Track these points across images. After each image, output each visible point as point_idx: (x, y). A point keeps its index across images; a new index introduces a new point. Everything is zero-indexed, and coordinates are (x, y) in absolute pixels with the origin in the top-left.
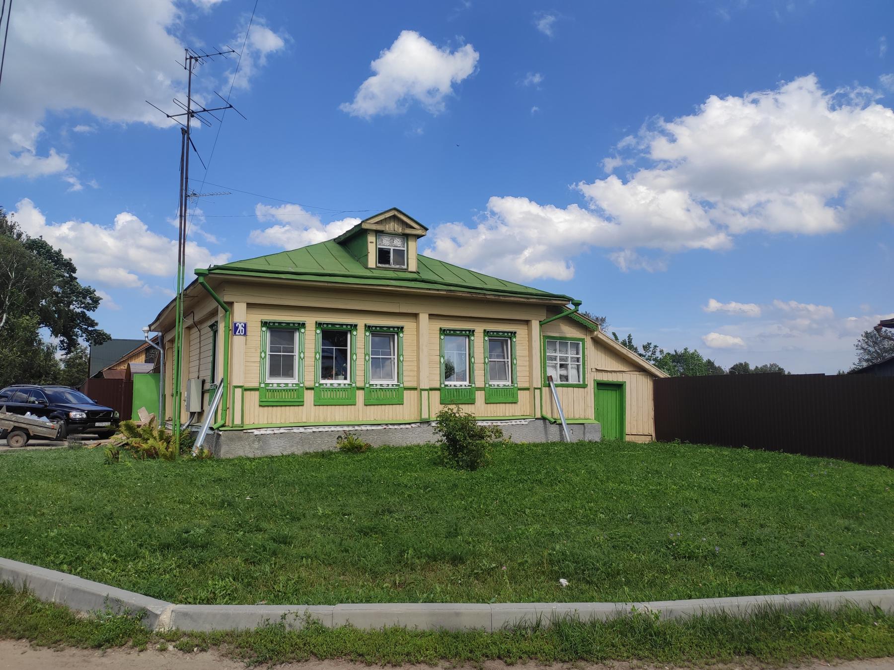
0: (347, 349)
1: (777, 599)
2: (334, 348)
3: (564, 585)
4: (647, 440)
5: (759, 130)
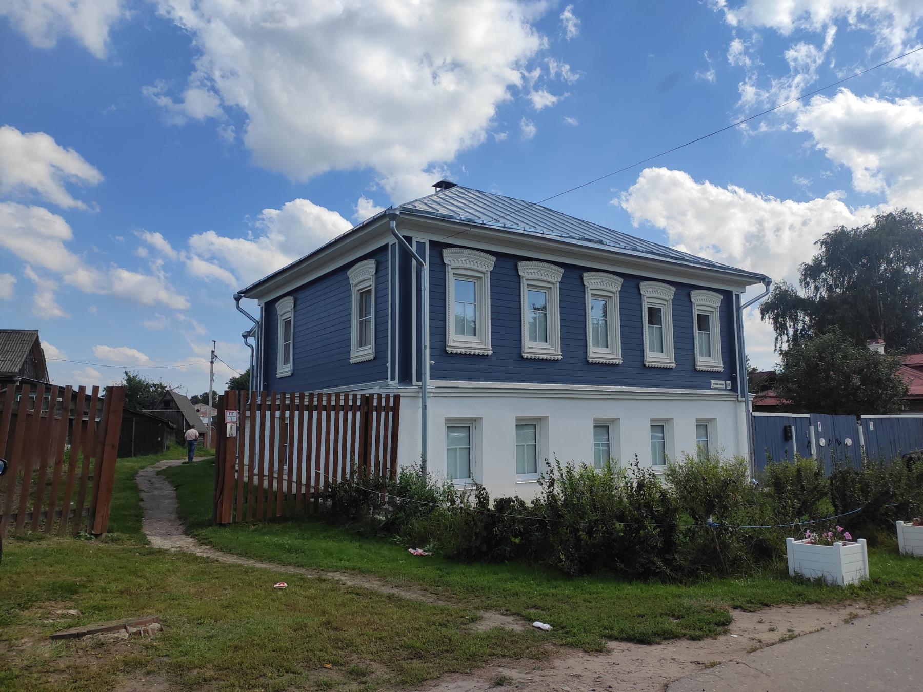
4: (395, 222)
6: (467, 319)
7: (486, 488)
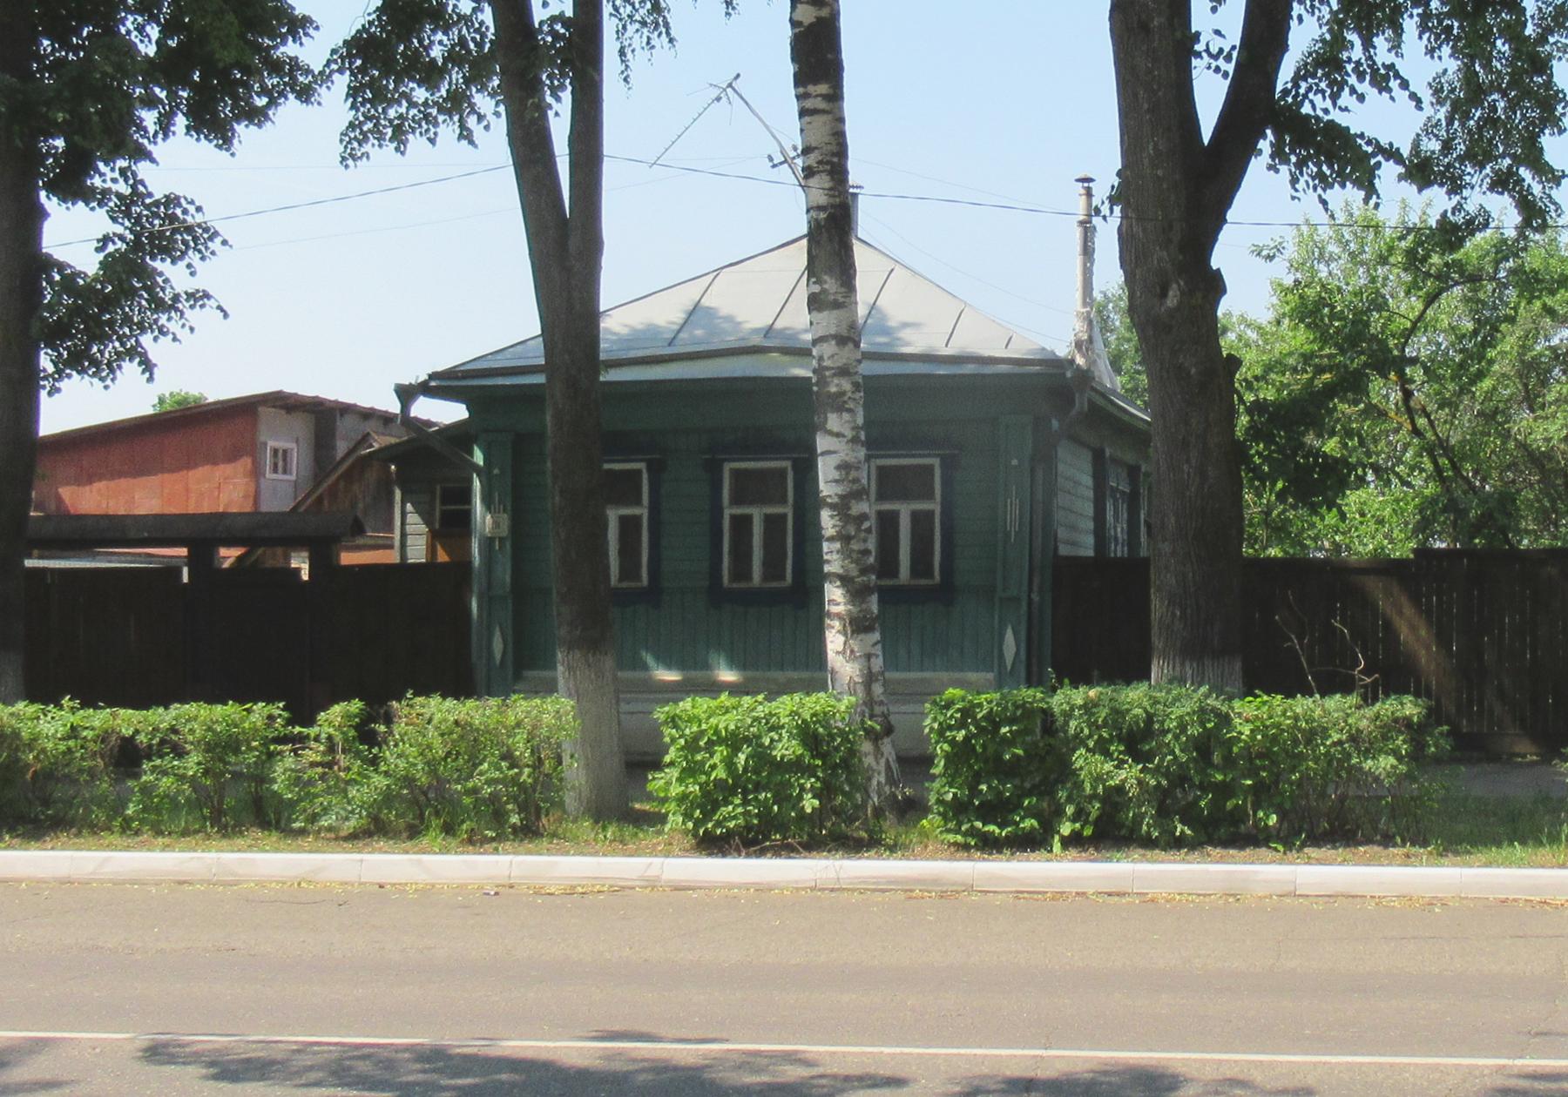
0: (784, 516)
1: (453, 507)
2: (727, 513)
5: (831, 539)
7: (196, 331)
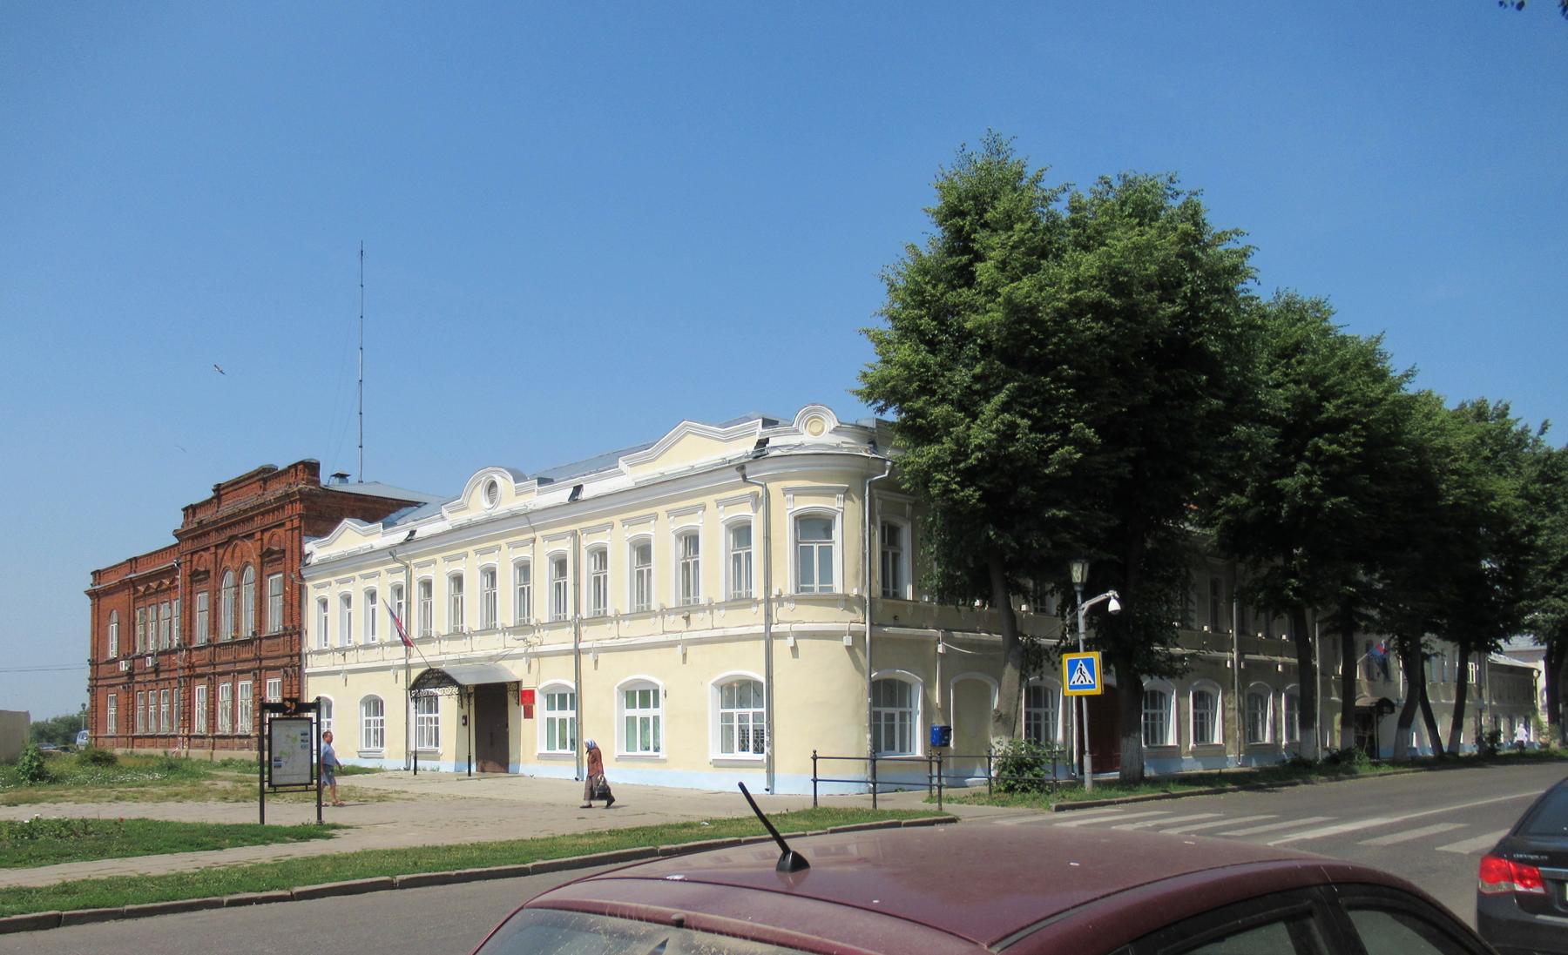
0: (555, 749)
3: (309, 547)
6: (1235, 742)
7: (1497, 5)
